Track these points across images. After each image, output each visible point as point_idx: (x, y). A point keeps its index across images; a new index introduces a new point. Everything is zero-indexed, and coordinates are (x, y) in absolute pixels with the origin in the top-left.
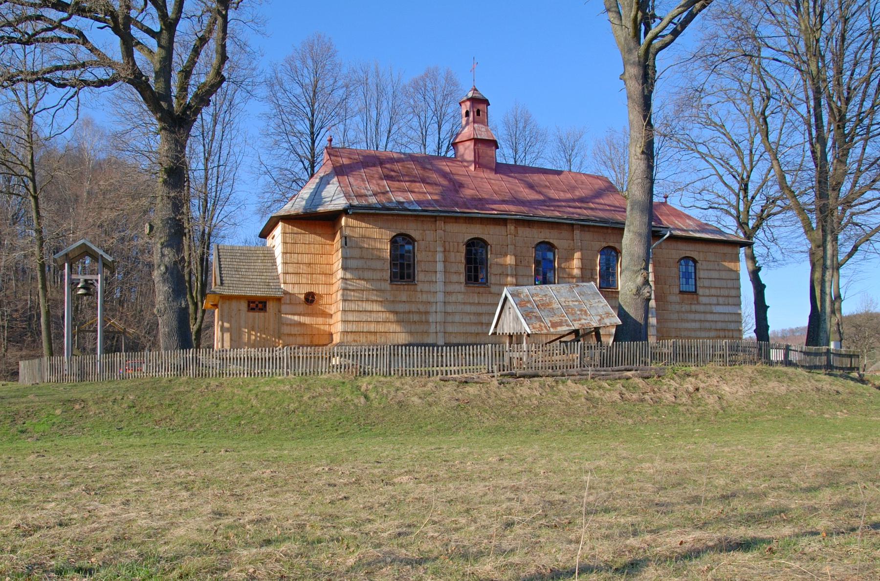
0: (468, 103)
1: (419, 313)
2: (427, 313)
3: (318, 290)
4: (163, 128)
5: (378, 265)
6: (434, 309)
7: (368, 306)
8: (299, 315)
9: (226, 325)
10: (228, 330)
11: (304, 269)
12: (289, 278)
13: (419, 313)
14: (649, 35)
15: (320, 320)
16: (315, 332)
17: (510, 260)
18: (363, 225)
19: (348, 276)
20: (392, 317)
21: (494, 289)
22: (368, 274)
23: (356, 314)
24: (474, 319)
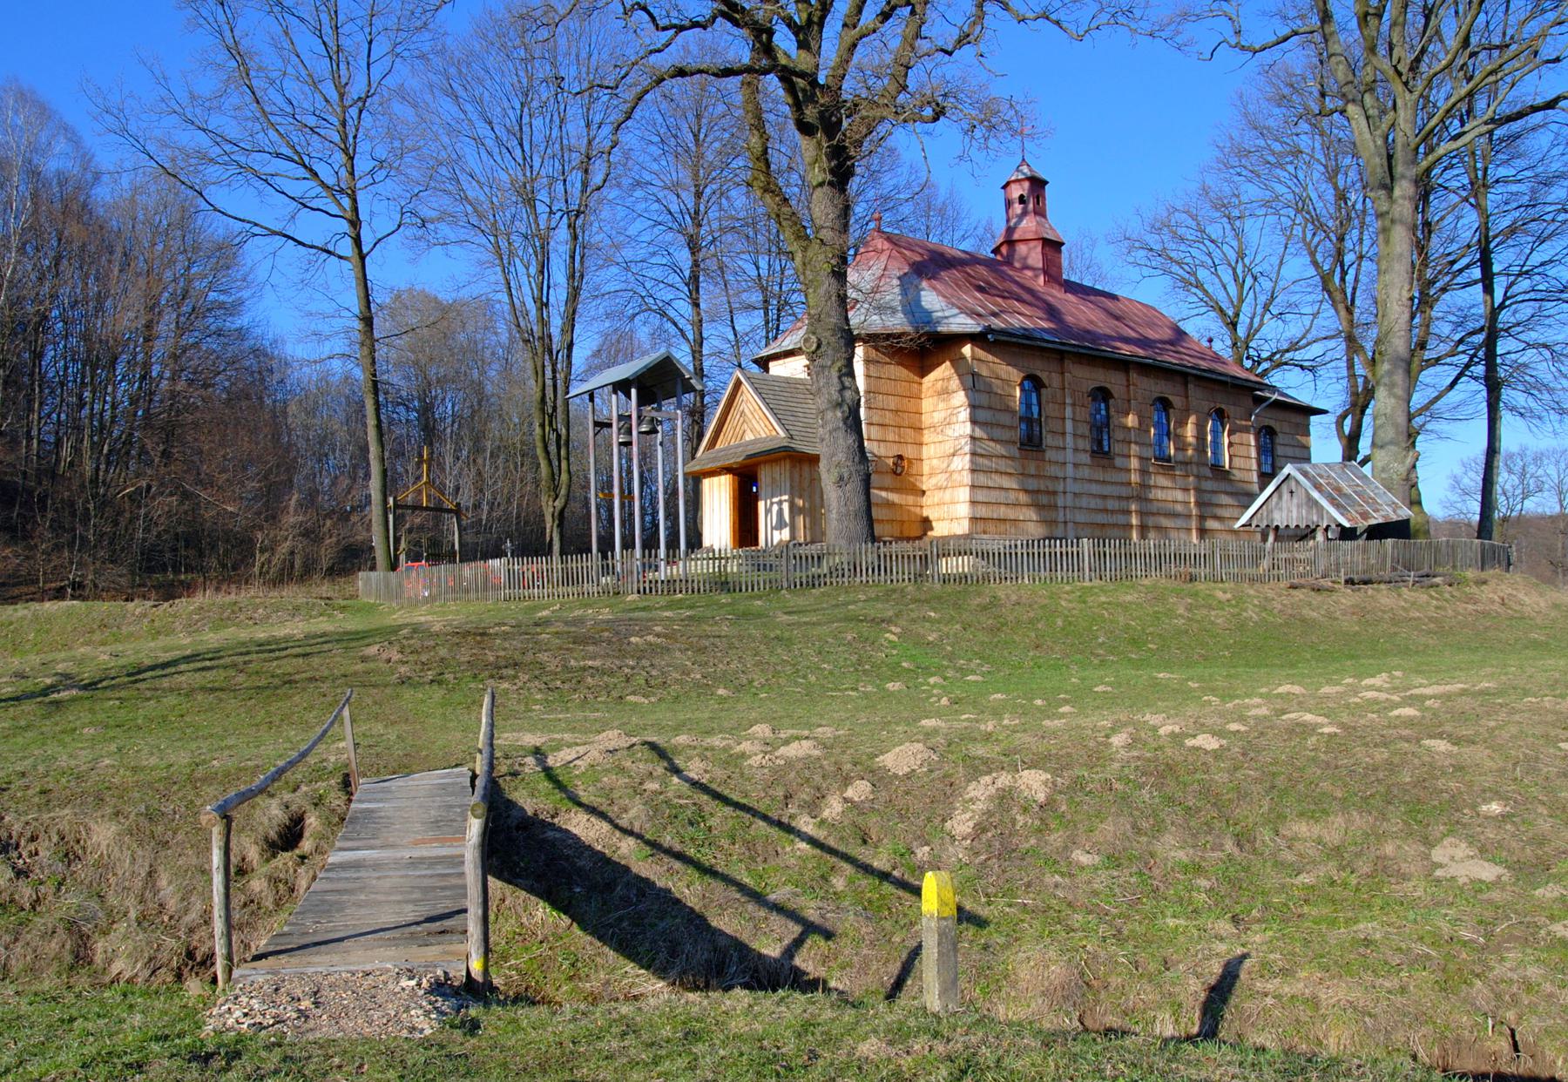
0: (1026, 185)
1: (1048, 492)
2: (1055, 493)
3: (909, 452)
4: (831, 184)
5: (1005, 419)
6: (1061, 488)
7: (998, 480)
8: (886, 489)
9: (800, 503)
10: (801, 511)
11: (889, 418)
12: (874, 429)
13: (1048, 492)
14: (1431, 158)
15: (910, 499)
16: (905, 518)
17: (1131, 420)
18: (990, 358)
19: (979, 433)
20: (1023, 498)
21: (1118, 462)
22: (997, 433)
23: (985, 491)
24: (1099, 503)
